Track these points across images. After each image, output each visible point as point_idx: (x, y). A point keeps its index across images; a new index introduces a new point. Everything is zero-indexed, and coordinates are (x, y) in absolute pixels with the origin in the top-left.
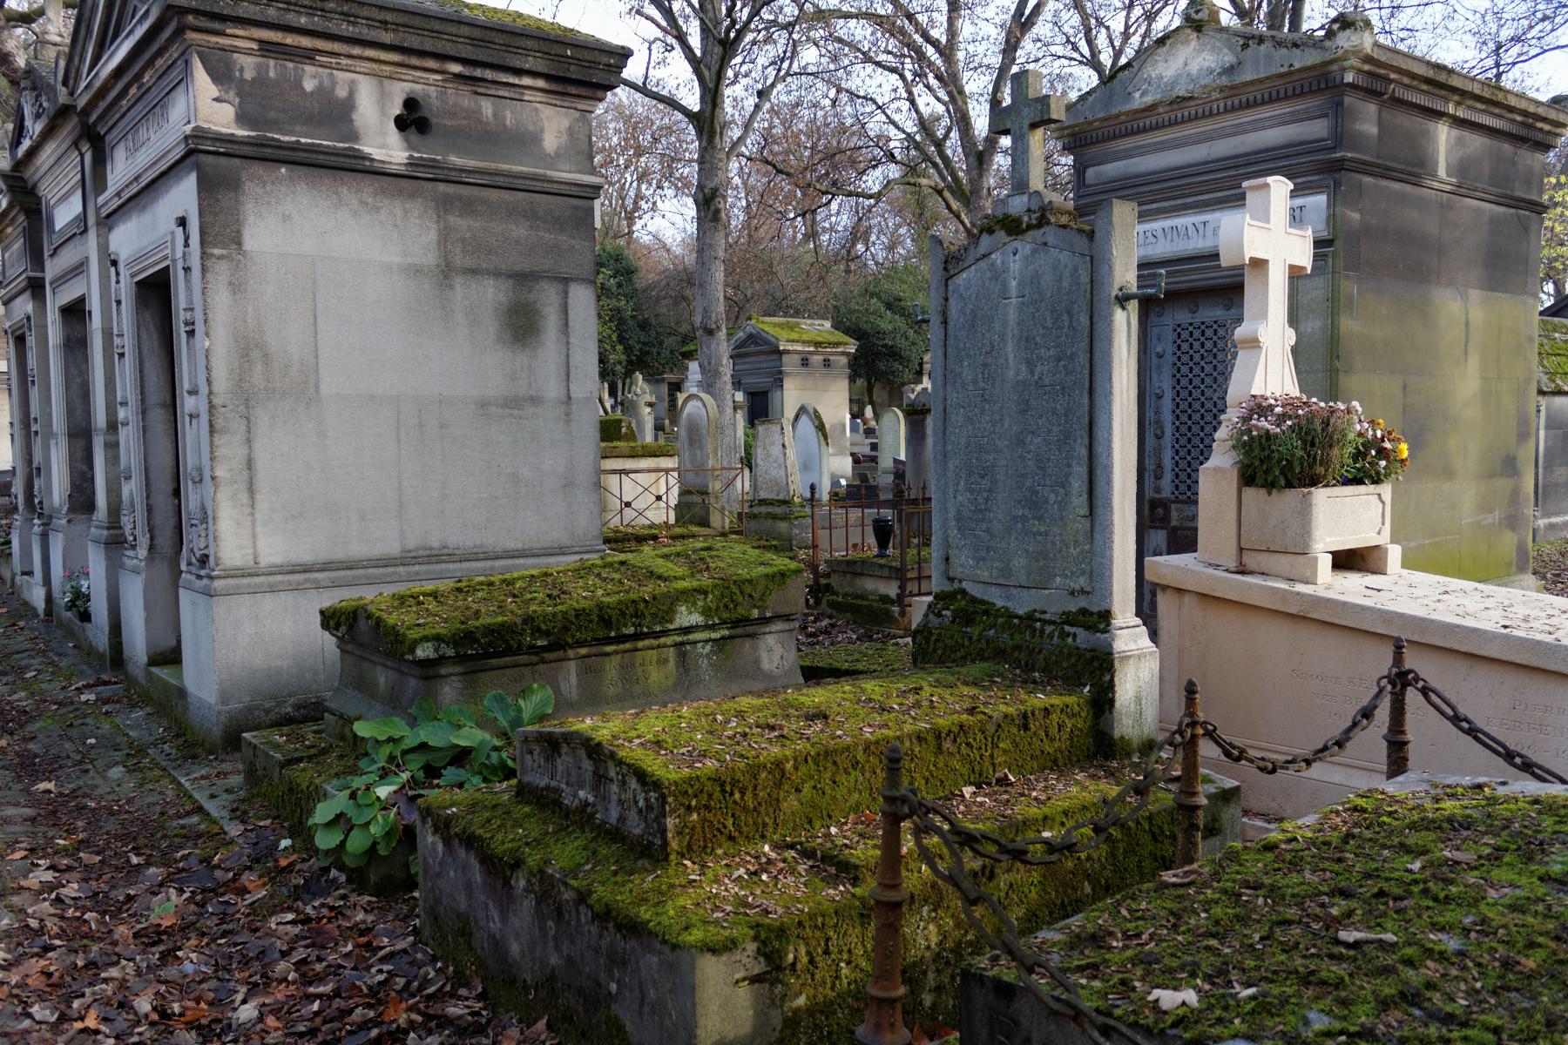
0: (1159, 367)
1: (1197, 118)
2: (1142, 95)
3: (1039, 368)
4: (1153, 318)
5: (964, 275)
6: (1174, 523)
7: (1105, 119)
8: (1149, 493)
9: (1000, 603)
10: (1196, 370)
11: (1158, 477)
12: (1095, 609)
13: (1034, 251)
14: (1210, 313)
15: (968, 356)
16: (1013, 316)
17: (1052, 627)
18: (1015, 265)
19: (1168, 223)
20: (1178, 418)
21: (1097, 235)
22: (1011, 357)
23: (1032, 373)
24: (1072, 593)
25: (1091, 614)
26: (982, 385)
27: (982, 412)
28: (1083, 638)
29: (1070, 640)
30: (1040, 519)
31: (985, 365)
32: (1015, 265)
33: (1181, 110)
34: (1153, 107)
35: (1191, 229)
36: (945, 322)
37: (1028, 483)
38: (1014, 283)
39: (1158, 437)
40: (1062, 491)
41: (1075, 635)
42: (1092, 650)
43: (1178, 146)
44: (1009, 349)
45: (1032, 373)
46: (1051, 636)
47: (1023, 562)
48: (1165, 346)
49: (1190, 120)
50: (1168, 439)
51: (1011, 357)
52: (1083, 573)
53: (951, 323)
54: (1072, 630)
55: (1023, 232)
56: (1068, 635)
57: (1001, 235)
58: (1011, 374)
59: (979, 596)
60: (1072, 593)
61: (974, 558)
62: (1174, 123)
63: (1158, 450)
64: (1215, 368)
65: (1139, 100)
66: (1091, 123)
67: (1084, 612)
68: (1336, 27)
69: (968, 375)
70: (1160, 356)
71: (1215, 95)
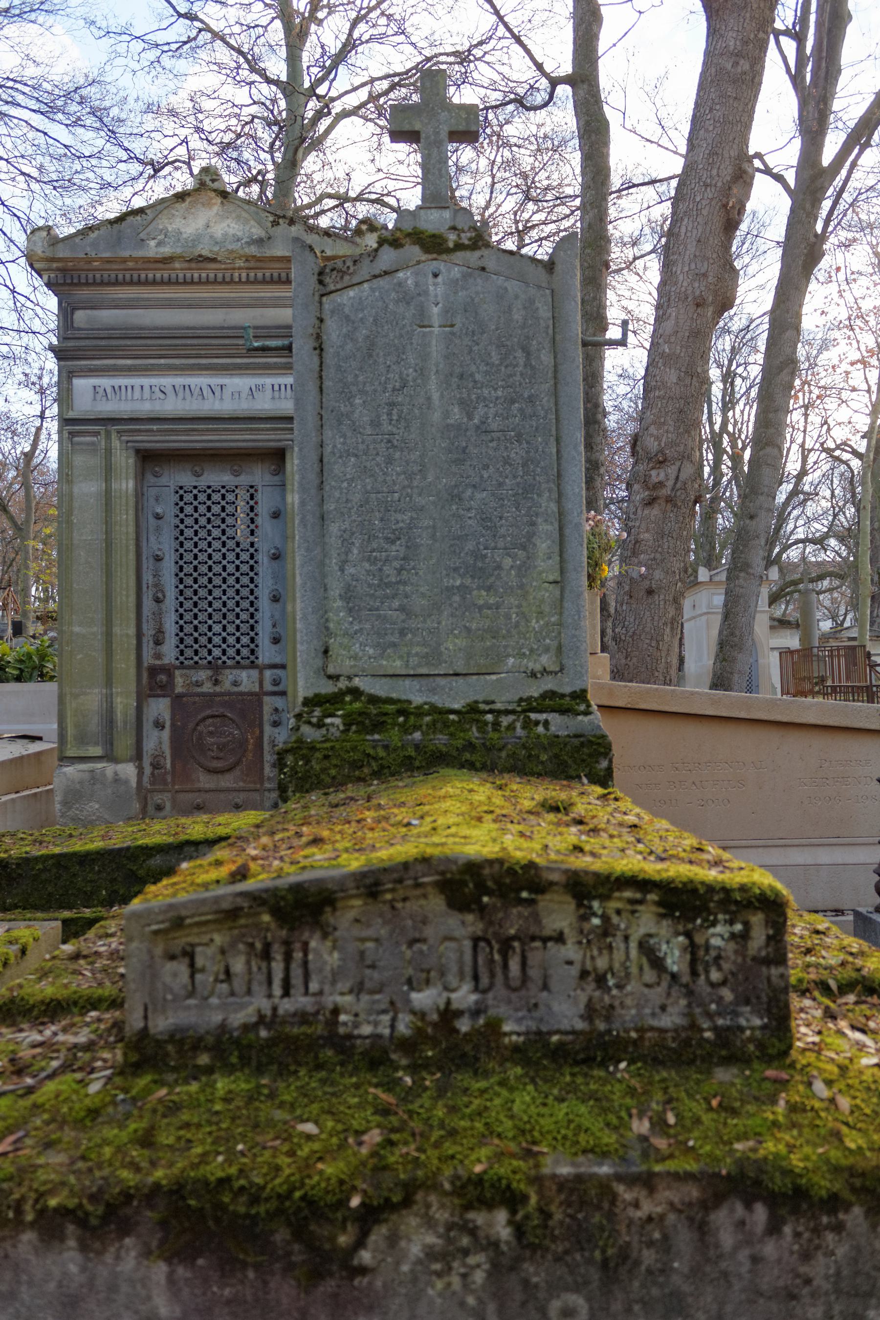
0: (158, 529)
1: (215, 282)
2: (159, 244)
3: (481, 410)
5: (351, 293)
6: (179, 690)
7: (108, 261)
8: (148, 659)
9: (417, 699)
10: (202, 534)
11: (158, 643)
12: (567, 690)
13: (465, 276)
14: (258, 475)
15: (362, 392)
16: (436, 349)
17: (511, 718)
18: (437, 289)
19: (179, 381)
20: (181, 581)
21: (559, 268)
25: (563, 696)
27: (389, 461)
28: (558, 724)
29: (540, 729)
30: (488, 589)
31: (392, 404)
32: (437, 289)
34: (167, 260)
36: (320, 349)
37: (470, 546)
38: (435, 310)
39: (158, 601)
41: (546, 723)
42: (576, 736)
43: (190, 306)
44: (433, 385)
45: (470, 417)
47: (461, 642)
48: (167, 508)
49: (208, 282)
51: (436, 396)
52: (547, 650)
53: (329, 352)
54: (543, 717)
55: (449, 251)
56: (537, 723)
57: (414, 251)
58: (436, 416)
60: (533, 675)
61: (377, 646)
63: (158, 616)
64: (224, 532)
65: (152, 249)
66: (90, 261)
67: (551, 694)
68: (364, 227)
69: (362, 415)
70: (158, 517)
71: (240, 263)
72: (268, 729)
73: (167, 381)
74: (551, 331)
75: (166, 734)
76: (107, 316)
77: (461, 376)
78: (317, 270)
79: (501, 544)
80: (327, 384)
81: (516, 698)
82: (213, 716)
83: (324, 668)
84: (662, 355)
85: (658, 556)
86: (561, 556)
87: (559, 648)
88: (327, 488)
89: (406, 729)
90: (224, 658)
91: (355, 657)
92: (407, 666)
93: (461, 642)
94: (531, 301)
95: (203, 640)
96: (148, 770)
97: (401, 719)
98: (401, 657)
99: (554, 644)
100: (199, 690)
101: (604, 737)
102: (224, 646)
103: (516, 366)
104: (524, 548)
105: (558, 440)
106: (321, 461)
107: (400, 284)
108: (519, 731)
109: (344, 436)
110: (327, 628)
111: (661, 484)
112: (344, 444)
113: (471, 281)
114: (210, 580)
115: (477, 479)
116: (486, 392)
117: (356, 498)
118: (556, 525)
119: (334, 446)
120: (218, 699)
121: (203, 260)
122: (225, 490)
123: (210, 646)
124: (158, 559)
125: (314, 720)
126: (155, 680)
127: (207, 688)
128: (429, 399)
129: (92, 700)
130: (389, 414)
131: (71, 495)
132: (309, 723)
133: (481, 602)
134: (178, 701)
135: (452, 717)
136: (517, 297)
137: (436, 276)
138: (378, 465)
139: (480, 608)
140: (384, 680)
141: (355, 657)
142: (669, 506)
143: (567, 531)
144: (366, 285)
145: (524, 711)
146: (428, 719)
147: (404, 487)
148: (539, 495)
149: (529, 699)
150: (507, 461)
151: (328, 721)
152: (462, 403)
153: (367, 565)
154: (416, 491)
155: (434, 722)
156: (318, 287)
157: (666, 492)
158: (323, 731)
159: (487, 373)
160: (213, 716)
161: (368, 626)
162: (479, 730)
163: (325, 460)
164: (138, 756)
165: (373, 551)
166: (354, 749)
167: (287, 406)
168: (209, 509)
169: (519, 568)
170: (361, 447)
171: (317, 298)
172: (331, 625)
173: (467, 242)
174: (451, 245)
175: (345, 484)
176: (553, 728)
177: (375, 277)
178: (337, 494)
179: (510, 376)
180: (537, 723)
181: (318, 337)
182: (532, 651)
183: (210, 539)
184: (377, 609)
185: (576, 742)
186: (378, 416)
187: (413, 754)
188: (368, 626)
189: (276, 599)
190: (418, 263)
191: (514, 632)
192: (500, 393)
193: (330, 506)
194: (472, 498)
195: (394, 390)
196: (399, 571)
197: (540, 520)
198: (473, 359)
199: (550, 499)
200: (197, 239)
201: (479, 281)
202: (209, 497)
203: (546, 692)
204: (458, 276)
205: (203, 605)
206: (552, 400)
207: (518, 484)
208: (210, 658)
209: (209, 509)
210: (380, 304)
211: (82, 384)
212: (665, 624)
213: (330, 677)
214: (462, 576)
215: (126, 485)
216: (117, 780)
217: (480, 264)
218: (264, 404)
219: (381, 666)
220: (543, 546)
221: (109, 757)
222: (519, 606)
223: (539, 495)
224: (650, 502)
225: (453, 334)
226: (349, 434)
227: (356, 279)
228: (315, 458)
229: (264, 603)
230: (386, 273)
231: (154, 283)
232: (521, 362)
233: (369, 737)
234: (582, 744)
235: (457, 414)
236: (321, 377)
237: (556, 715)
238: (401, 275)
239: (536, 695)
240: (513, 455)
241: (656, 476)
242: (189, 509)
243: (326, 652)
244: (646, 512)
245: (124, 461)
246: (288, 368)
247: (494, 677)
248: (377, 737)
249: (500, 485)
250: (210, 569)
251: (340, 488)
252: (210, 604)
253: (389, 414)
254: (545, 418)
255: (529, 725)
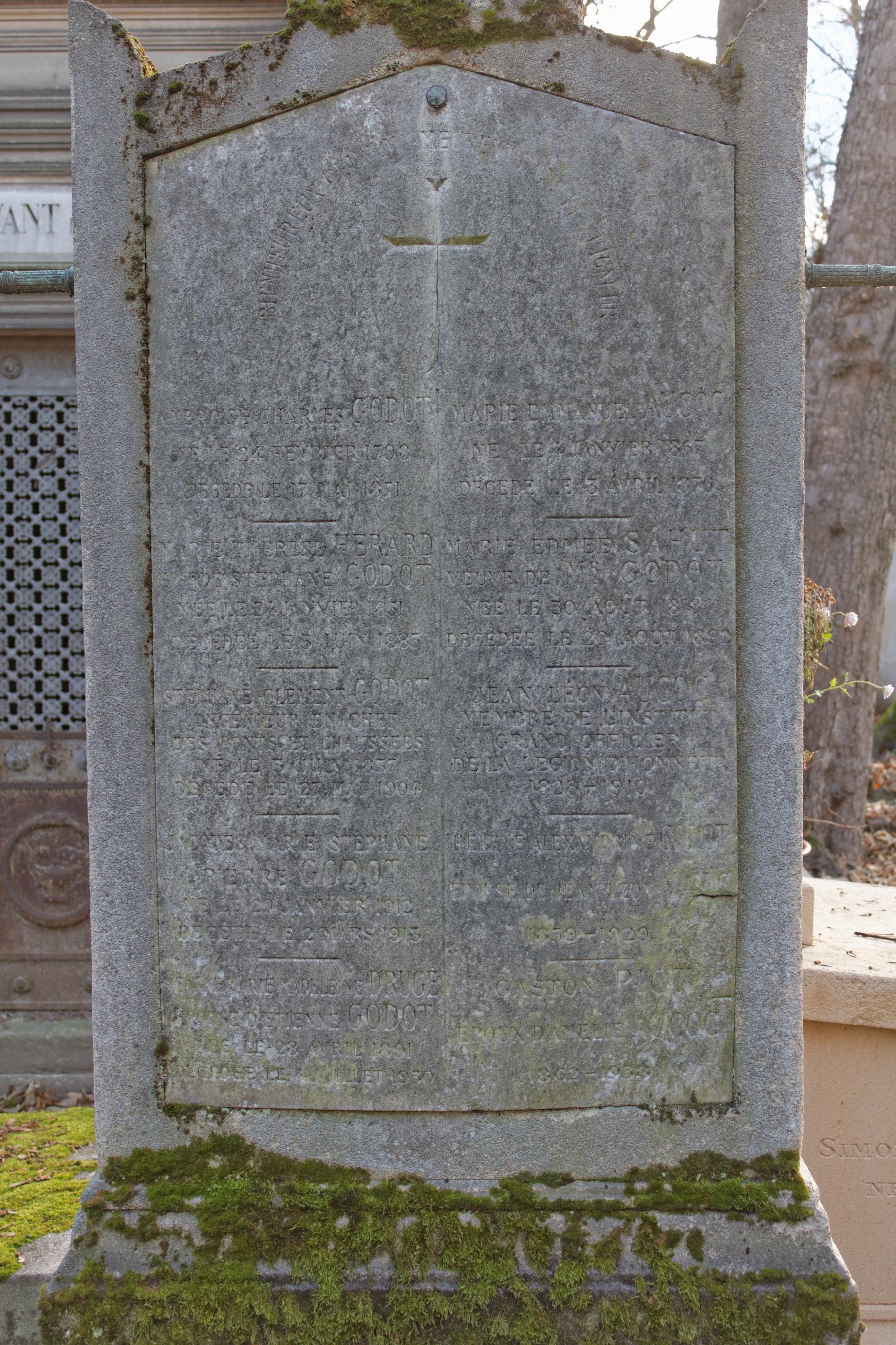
3: (548, 461)
5: (222, 151)
9: (384, 1169)
12: (749, 1152)
13: (511, 109)
17: (611, 1224)
18: (440, 143)
21: (753, 87)
22: (433, 423)
23: (519, 478)
24: (666, 1114)
25: (738, 1166)
26: (309, 503)
27: (317, 586)
28: (727, 1244)
29: (681, 1254)
30: (559, 911)
31: (323, 443)
32: (440, 143)
35: (21, 217)
37: (515, 803)
38: (435, 198)
40: (643, 826)
41: (696, 1241)
42: (767, 1279)
44: (426, 393)
45: (519, 478)
46: (609, 1249)
47: (491, 1039)
51: (433, 423)
52: (701, 1053)
54: (688, 1223)
55: (470, 41)
56: (673, 1240)
58: (435, 475)
59: (298, 1153)
60: (666, 1114)
74: (729, 257)
77: (498, 374)
78: (132, 92)
79: (592, 801)
80: (161, 387)
81: (623, 1170)
82: (45, 827)
83: (158, 1088)
84: (874, 105)
85: (853, 468)
86: (740, 830)
87: (732, 1049)
88: (162, 652)
89: (353, 1251)
90: (66, 720)
91: (232, 1066)
92: (358, 1091)
93: (491, 1039)
94: (682, 176)
95: (26, 686)
97: (343, 1222)
98: (343, 1070)
99: (721, 1039)
100: (19, 777)
101: (839, 1282)
102: (65, 697)
103: (640, 346)
104: (650, 812)
105: (740, 539)
106: (148, 583)
107: (345, 129)
108: (631, 1260)
109: (205, 523)
110: (165, 995)
111: (864, 341)
112: (203, 541)
113: (527, 120)
114: (38, 575)
115: (535, 637)
116: (560, 413)
117: (234, 680)
118: (732, 755)
119: (180, 548)
120: (54, 794)
123: (39, 697)
125: (132, 1221)
127: (36, 773)
128: (416, 429)
130: (317, 468)
132: (121, 1228)
133: (541, 942)
135: (465, 1218)
136: (643, 165)
137: (437, 106)
138: (288, 596)
139: (538, 957)
140: (302, 1120)
141: (232, 1066)
142: (876, 381)
143: (758, 766)
144: (258, 130)
145: (642, 1207)
146: (407, 1222)
147: (352, 654)
148: (691, 680)
149: (654, 1174)
150: (610, 593)
151: (166, 1222)
152: (498, 439)
153: (260, 845)
154: (381, 662)
155: (421, 1234)
156: (136, 134)
157: (871, 354)
158: (154, 1248)
159: (563, 364)
160: (45, 827)
161: (262, 992)
162: (535, 1255)
163: (157, 582)
165: (278, 810)
166: (227, 1302)
168: (34, 440)
169: (637, 860)
170: (246, 550)
171: (133, 163)
172: (175, 988)
173: (517, 18)
174: (476, 24)
175: (206, 644)
176: (711, 1253)
177: (282, 108)
178: (187, 668)
179: (623, 373)
180: (673, 1240)
181: (139, 265)
182: (662, 1056)
183: (36, 496)
184: (286, 954)
185: (769, 1294)
186: (289, 473)
187: (370, 1320)
188: (262, 992)
190: (393, 71)
191: (620, 1013)
192: (595, 418)
193: (169, 697)
194: (520, 684)
195: (328, 405)
196: (340, 862)
197: (690, 742)
198: (528, 328)
199: (716, 690)
201: (547, 119)
202: (33, 418)
203: (694, 1157)
204: (495, 107)
205: (25, 620)
206: (729, 438)
207: (638, 650)
208: (39, 719)
209: (34, 440)
210: (294, 180)
212: (861, 586)
213: (171, 1111)
214: (495, 880)
217: (551, 75)
219: (295, 1088)
220: (696, 808)
222: (635, 952)
223: (691, 680)
224: (843, 372)
225: (479, 261)
226: (216, 517)
227: (233, 116)
228: (133, 574)
230: (309, 98)
232: (652, 337)
233: (263, 1269)
234: (785, 1303)
236: (145, 371)
237: (720, 1219)
238: (347, 102)
239: (671, 1163)
240: (626, 576)
241: (854, 327)
243: (162, 1050)
244: (835, 389)
247: (569, 1118)
248: (282, 1267)
249: (593, 651)
250: (37, 553)
251: (195, 653)
252: (38, 619)
253: (317, 468)
254: (708, 483)
255: (652, 1242)
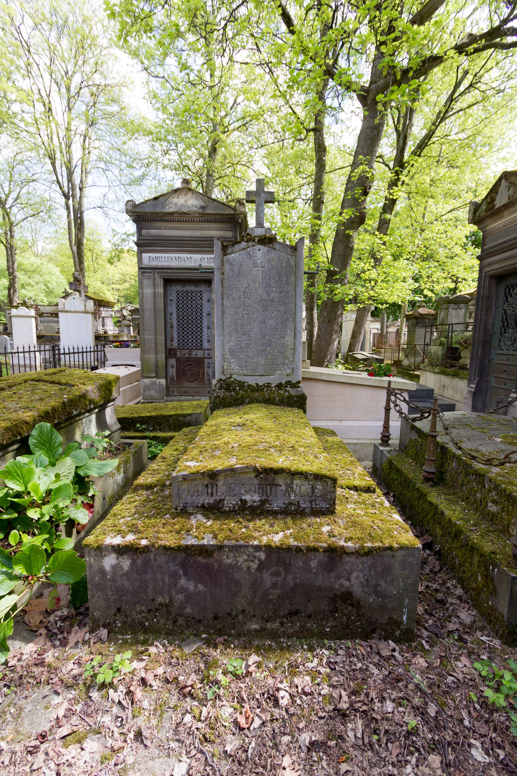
4: (169, 288)
11: (172, 341)
14: (203, 288)
19: (177, 255)
33: (181, 217)
34: (172, 214)
50: (175, 328)
62: (180, 221)
72: (206, 369)
73: (173, 255)
75: (175, 369)
76: (153, 232)
94: (289, 260)
96: (169, 381)
121: (184, 213)
122: (192, 292)
124: (171, 314)
126: (170, 353)
129: (152, 357)
131: (143, 293)
134: (178, 360)
152: (266, 292)
164: (166, 377)
167: (212, 265)
189: (208, 328)
200: (182, 206)
211: (145, 256)
215: (161, 290)
216: (160, 384)
218: (205, 264)
221: (157, 377)
229: (205, 329)
231: (168, 221)
235: (265, 296)
242: (181, 298)
245: (160, 282)
246: (212, 252)
